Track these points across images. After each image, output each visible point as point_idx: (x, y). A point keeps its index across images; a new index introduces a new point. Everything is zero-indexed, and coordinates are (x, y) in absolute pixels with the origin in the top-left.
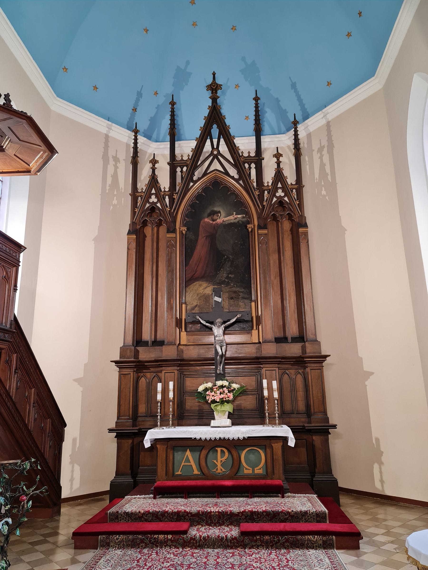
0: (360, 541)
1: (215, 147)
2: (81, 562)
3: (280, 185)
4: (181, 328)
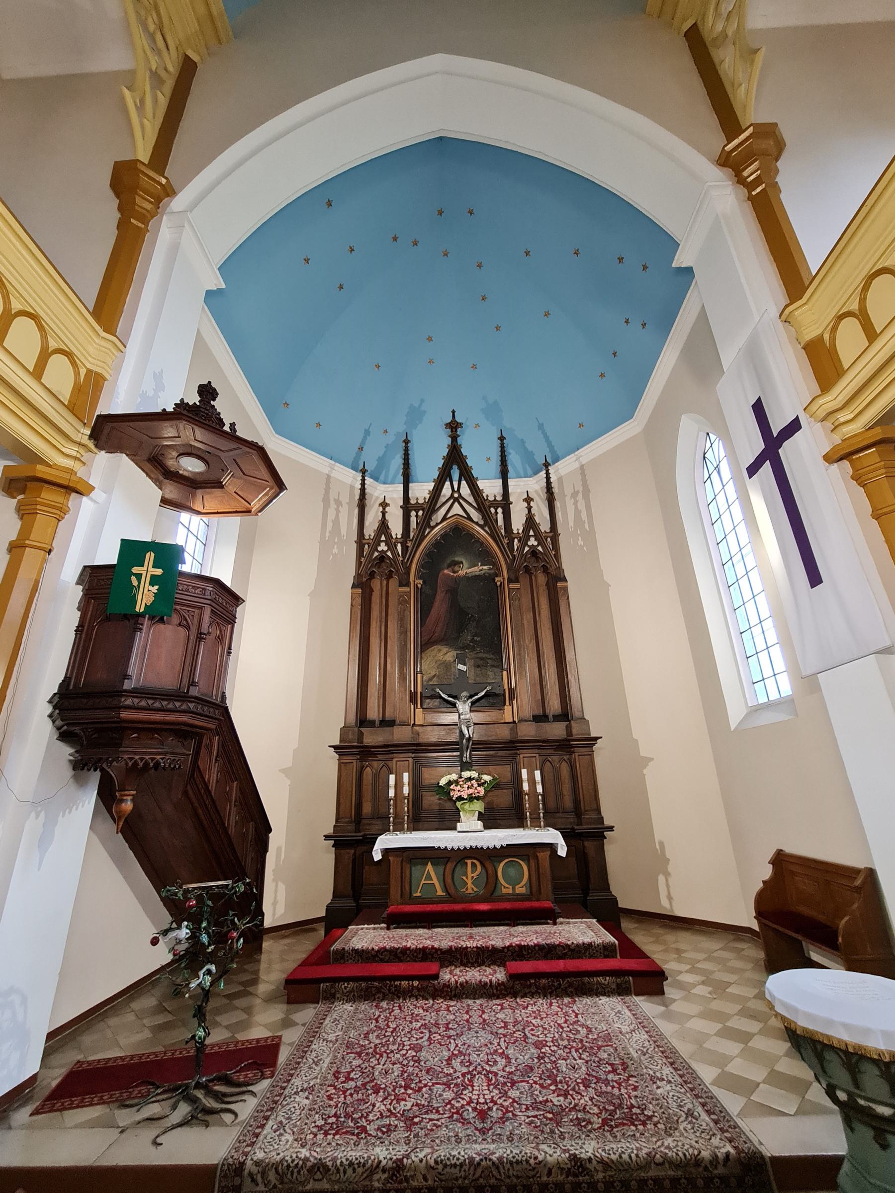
0: (664, 983)
1: (456, 489)
2: (298, 1024)
3: (531, 533)
4: (415, 703)
